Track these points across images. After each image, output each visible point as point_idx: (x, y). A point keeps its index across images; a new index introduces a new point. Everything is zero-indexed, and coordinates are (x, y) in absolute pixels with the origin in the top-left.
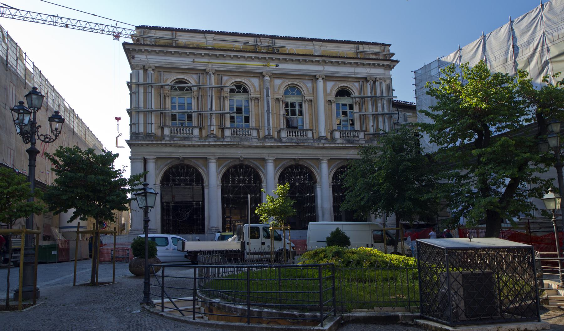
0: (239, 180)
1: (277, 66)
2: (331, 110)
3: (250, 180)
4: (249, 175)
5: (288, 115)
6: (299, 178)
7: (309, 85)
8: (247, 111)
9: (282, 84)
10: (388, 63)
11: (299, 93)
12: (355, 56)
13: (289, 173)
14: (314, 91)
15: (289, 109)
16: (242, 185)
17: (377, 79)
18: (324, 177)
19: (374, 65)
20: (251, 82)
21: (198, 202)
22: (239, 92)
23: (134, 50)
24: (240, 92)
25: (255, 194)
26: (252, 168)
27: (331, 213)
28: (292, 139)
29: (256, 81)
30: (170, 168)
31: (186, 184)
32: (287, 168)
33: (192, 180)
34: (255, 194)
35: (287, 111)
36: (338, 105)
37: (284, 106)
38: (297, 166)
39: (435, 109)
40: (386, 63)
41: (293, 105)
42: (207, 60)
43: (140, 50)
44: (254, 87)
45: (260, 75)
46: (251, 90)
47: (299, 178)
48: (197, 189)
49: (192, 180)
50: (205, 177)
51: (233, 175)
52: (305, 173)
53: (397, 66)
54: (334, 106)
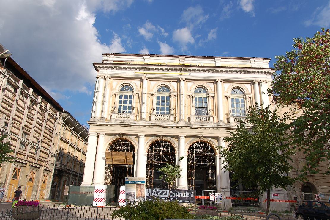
0: (160, 151)
2: (110, 98)
3: (207, 152)
4: (207, 148)
11: (131, 88)
13: (196, 147)
14: (216, 90)
16: (161, 154)
17: (262, 81)
18: (183, 150)
21: (130, 166)
23: (99, 67)
24: (164, 91)
26: (169, 143)
27: (227, 179)
28: (198, 122)
29: (138, 82)
36: (232, 100)
37: (194, 100)
41: (163, 98)
42: (144, 72)
43: (103, 67)
44: (137, 86)
45: (178, 81)
46: (135, 89)
51: (156, 147)
52: (168, 146)
54: (230, 100)
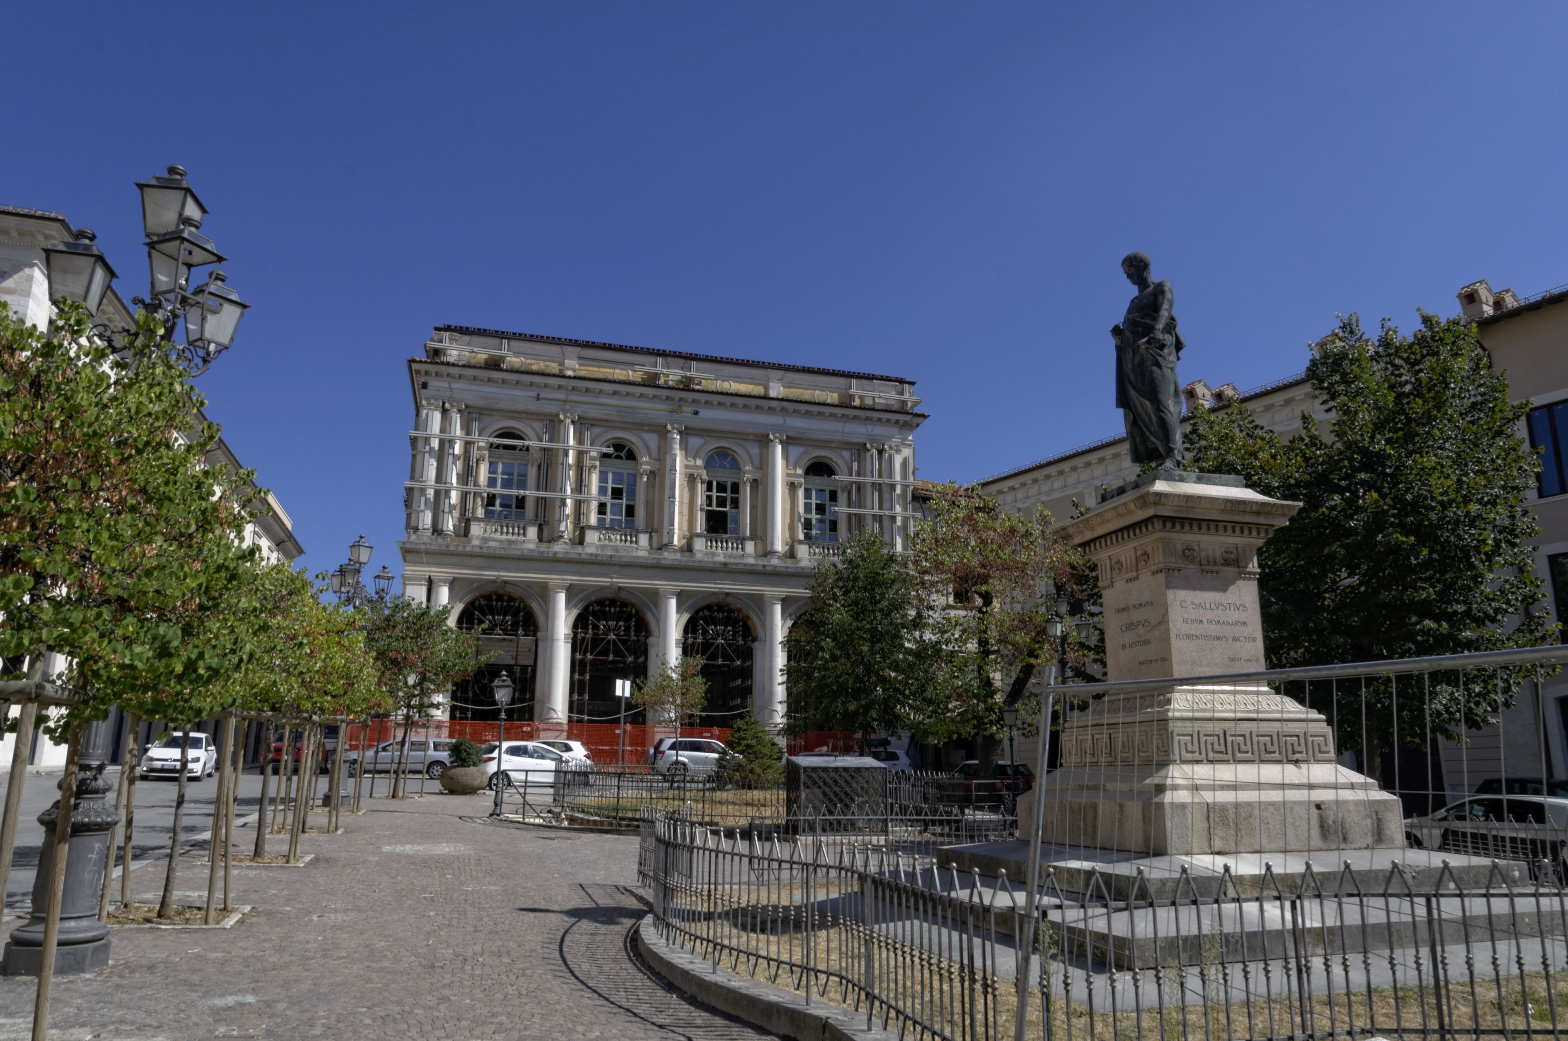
0: (608, 630)
1: (696, 413)
3: (627, 629)
4: (627, 620)
5: (710, 505)
6: (723, 635)
7: (755, 450)
8: (632, 493)
9: (702, 446)
10: (907, 418)
12: (1119, 1006)
15: (714, 494)
19: (879, 420)
20: (642, 439)
21: (524, 668)
22: (619, 457)
25: (636, 658)
26: (633, 606)
30: (477, 599)
31: (505, 631)
32: (702, 609)
33: (515, 626)
34: (636, 658)
35: (709, 498)
38: (720, 607)
39: (137, 301)
40: (903, 418)
47: (723, 635)
48: (526, 641)
49: (515, 626)
50: (541, 619)
53: (925, 424)
